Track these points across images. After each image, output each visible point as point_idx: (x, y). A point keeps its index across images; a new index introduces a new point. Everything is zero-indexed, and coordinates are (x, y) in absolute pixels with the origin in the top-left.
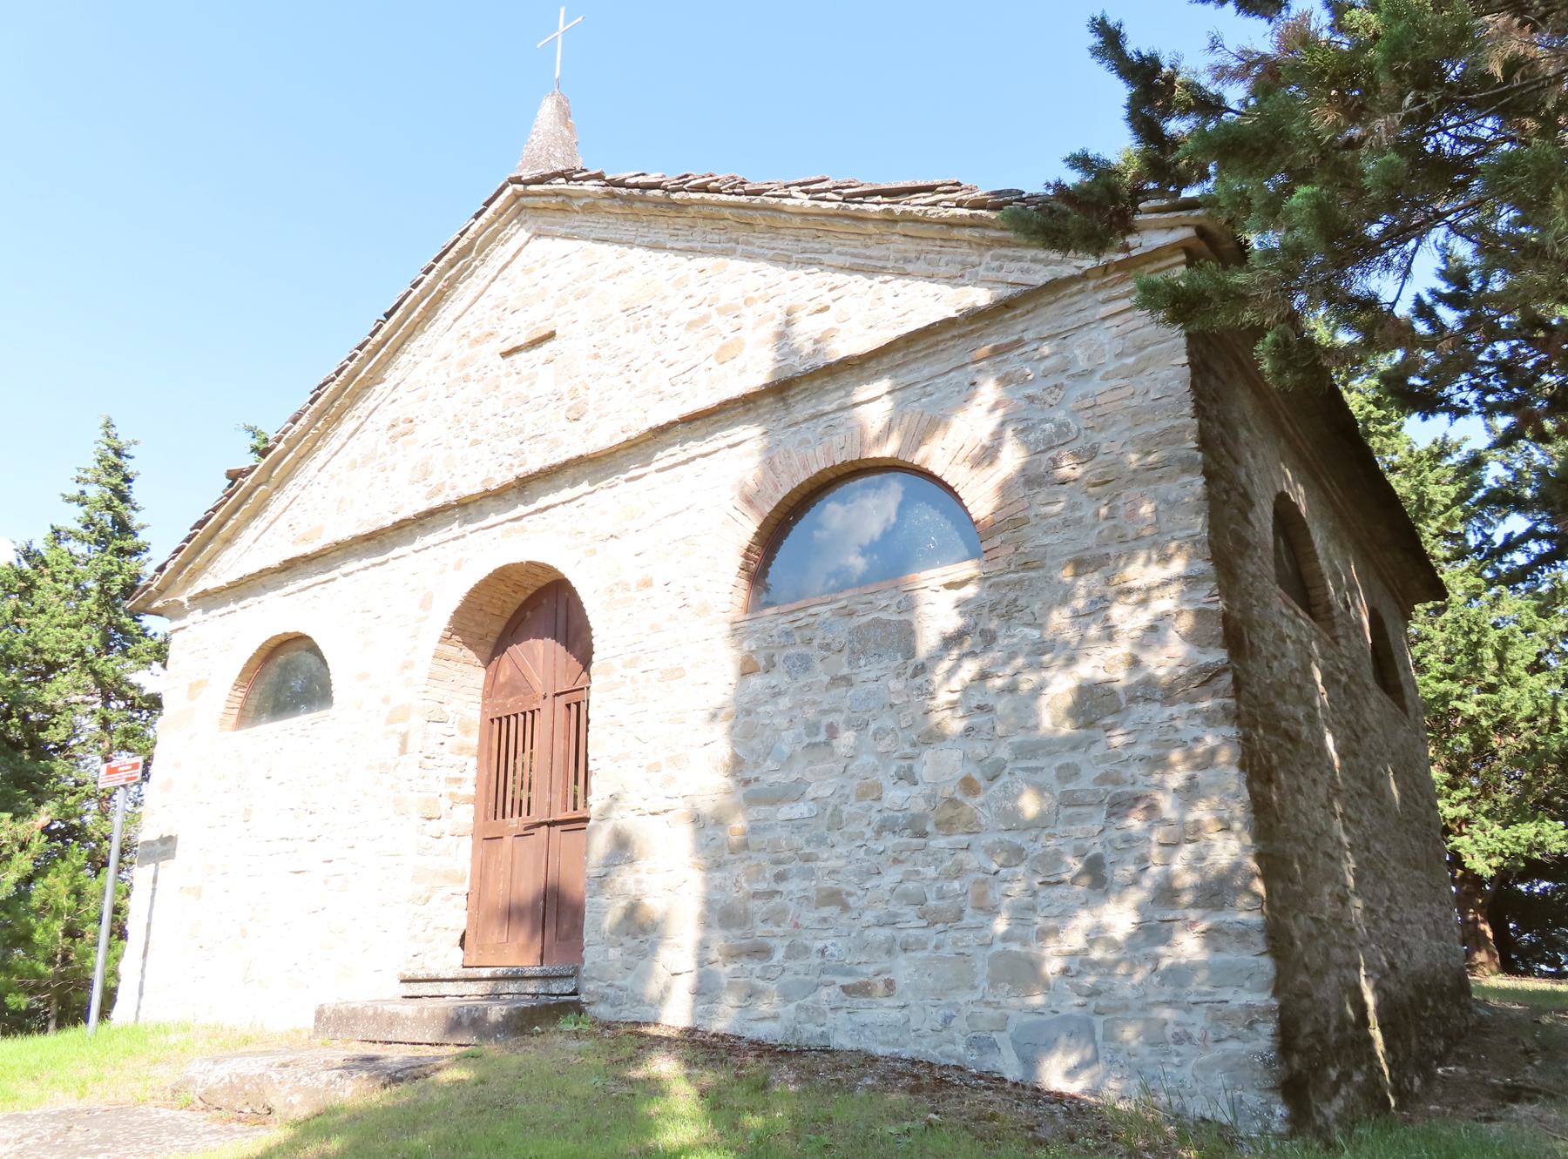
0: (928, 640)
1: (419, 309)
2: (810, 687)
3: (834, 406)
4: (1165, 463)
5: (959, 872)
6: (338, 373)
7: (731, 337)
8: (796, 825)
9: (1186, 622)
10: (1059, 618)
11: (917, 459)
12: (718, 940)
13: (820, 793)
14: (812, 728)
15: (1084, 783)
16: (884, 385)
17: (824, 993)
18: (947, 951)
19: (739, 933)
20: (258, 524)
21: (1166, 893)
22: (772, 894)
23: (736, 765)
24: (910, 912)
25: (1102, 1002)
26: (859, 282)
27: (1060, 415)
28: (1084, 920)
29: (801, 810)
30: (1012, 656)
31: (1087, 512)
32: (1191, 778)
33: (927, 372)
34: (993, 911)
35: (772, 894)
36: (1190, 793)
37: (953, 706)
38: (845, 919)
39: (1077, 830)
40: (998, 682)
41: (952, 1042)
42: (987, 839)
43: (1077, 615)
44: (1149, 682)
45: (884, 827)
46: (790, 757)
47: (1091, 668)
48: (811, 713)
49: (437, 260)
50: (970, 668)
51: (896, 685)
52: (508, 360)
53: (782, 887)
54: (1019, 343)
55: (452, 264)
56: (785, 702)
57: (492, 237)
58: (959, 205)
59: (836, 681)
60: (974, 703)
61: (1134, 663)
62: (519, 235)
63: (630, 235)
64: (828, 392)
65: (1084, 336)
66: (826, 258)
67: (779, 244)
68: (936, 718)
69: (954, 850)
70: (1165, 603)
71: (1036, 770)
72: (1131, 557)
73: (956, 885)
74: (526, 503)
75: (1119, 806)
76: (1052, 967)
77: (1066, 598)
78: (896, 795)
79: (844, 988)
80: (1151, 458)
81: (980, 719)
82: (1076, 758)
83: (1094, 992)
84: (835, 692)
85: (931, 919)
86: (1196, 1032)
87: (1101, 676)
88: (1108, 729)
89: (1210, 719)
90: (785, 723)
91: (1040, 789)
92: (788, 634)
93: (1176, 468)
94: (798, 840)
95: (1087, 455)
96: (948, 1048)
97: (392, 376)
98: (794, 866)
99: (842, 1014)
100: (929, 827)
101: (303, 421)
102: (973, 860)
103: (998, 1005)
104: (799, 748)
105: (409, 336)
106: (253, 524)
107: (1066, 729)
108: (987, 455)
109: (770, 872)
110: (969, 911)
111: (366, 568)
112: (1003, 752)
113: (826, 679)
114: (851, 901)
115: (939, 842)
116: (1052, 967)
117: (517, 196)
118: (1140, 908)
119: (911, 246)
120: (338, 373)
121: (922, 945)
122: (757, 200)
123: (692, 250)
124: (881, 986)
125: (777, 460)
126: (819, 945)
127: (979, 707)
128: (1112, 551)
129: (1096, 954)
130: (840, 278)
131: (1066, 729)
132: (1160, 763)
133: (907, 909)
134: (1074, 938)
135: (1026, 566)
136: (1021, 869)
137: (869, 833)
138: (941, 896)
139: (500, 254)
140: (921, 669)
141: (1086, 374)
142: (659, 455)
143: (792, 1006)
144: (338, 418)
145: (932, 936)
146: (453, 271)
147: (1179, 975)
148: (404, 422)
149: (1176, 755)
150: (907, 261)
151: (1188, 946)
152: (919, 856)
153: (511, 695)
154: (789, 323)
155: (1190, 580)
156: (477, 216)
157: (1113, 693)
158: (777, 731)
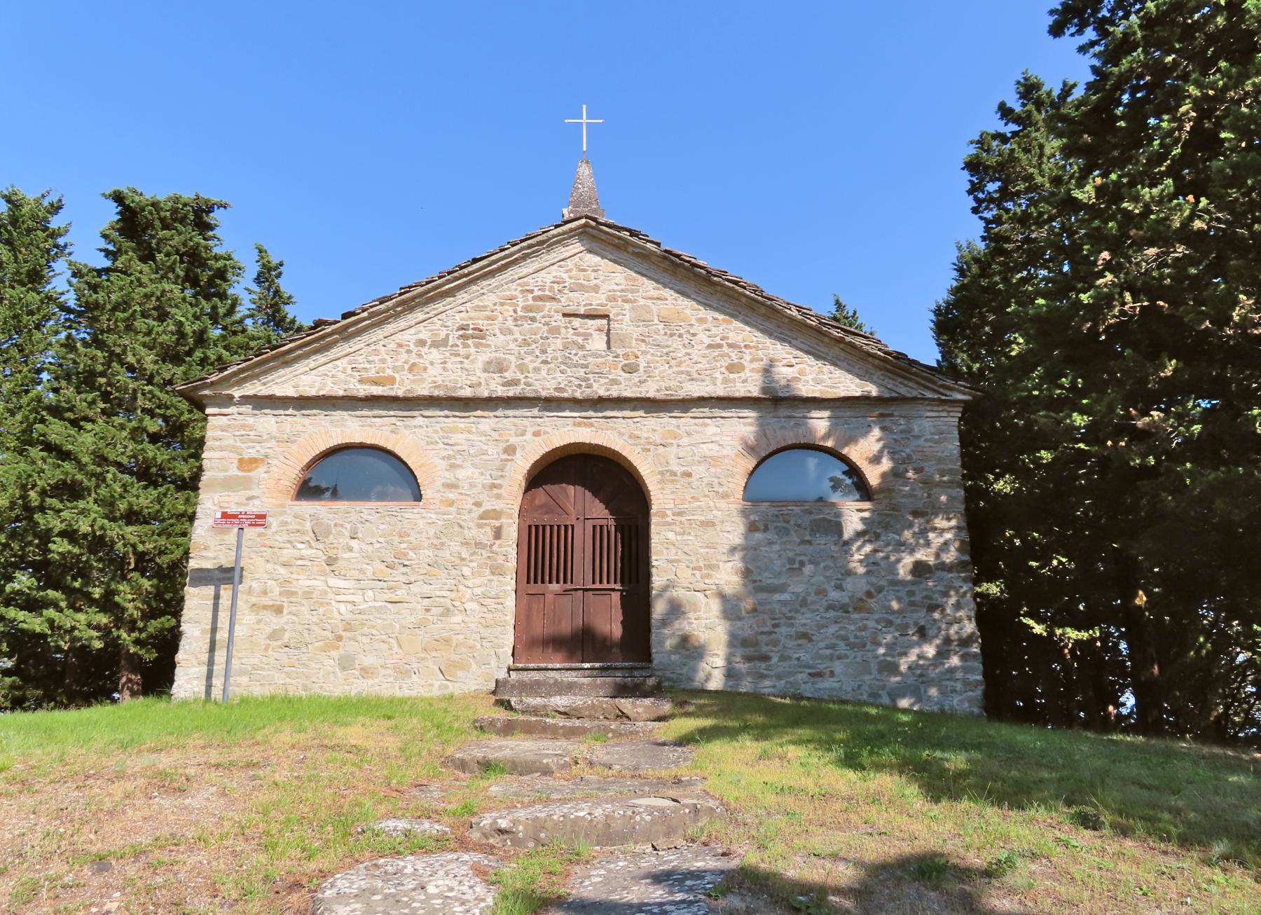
0: (848, 533)
1: (499, 264)
2: (790, 542)
3: (800, 415)
4: (951, 482)
5: (865, 628)
6: (428, 283)
7: (736, 361)
8: (784, 603)
9: (957, 544)
10: (907, 534)
11: (845, 451)
12: (739, 652)
13: (796, 590)
14: (791, 561)
15: (918, 598)
16: (826, 414)
17: (800, 676)
18: (859, 659)
19: (752, 649)
20: (320, 358)
21: (947, 641)
22: (771, 633)
23: (747, 573)
24: (842, 644)
25: (924, 679)
26: (810, 360)
27: (908, 451)
28: (916, 651)
29: (785, 597)
30: (888, 545)
31: (919, 493)
32: (958, 601)
33: (848, 414)
34: (879, 644)
35: (771, 633)
36: (958, 606)
37: (861, 561)
38: (809, 645)
39: (915, 615)
40: (881, 554)
41: (862, 695)
42: (877, 616)
43: (914, 533)
44: (943, 563)
45: (830, 607)
46: (779, 573)
47: (921, 555)
48: (791, 554)
49: (522, 241)
50: (868, 548)
51: (834, 548)
52: (567, 319)
53: (776, 630)
54: (891, 415)
55: (529, 247)
56: (776, 547)
57: (561, 241)
58: (880, 350)
59: (803, 542)
60: (871, 561)
61: (937, 556)
62: (576, 246)
63: (667, 280)
64: (798, 408)
65: (919, 421)
66: (794, 342)
67: (768, 325)
68: (852, 565)
69: (862, 619)
70: (948, 536)
71: (898, 591)
72: (937, 515)
73: (863, 633)
74: (596, 411)
75: (932, 608)
76: (903, 668)
77: (910, 526)
78: (834, 595)
79: (810, 674)
80: (945, 479)
81: (873, 568)
82: (914, 588)
83: (921, 675)
84: (803, 547)
85: (851, 646)
86: (958, 689)
87: (924, 558)
88: (927, 578)
89: (965, 580)
90: (776, 556)
91: (899, 600)
92: (777, 516)
93: (955, 485)
94: (784, 610)
95: (918, 470)
96: (860, 697)
97: (462, 296)
98: (783, 621)
99: (810, 684)
100: (851, 609)
101: (390, 304)
102: (871, 624)
103: (882, 681)
104: (784, 569)
105: (484, 277)
106: (314, 357)
107: (909, 578)
108: (876, 460)
109: (770, 623)
110: (869, 644)
111: (447, 417)
112: (883, 583)
113: (799, 541)
114: (814, 638)
115: (856, 616)
116: (903, 668)
117: (585, 225)
118: (937, 646)
119: (843, 355)
120: (428, 283)
121: (846, 657)
122: (769, 302)
123: (710, 306)
124: (828, 673)
125: (768, 432)
126: (797, 656)
127: (874, 563)
128: (929, 511)
129: (921, 662)
130: (800, 354)
131: (909, 578)
132: (946, 594)
133: (839, 642)
134: (912, 657)
135: (893, 509)
136: (892, 629)
137: (822, 610)
138: (856, 637)
139: (562, 252)
140: (847, 543)
141: (918, 437)
142: (694, 410)
143: (783, 682)
144: (411, 309)
145: (851, 654)
146: (529, 251)
147: (952, 670)
148: (473, 329)
149: (952, 593)
150: (839, 360)
151: (955, 661)
152: (846, 621)
153: (547, 513)
154: (771, 366)
155: (958, 528)
156: (557, 226)
157: (929, 565)
158: (771, 560)
